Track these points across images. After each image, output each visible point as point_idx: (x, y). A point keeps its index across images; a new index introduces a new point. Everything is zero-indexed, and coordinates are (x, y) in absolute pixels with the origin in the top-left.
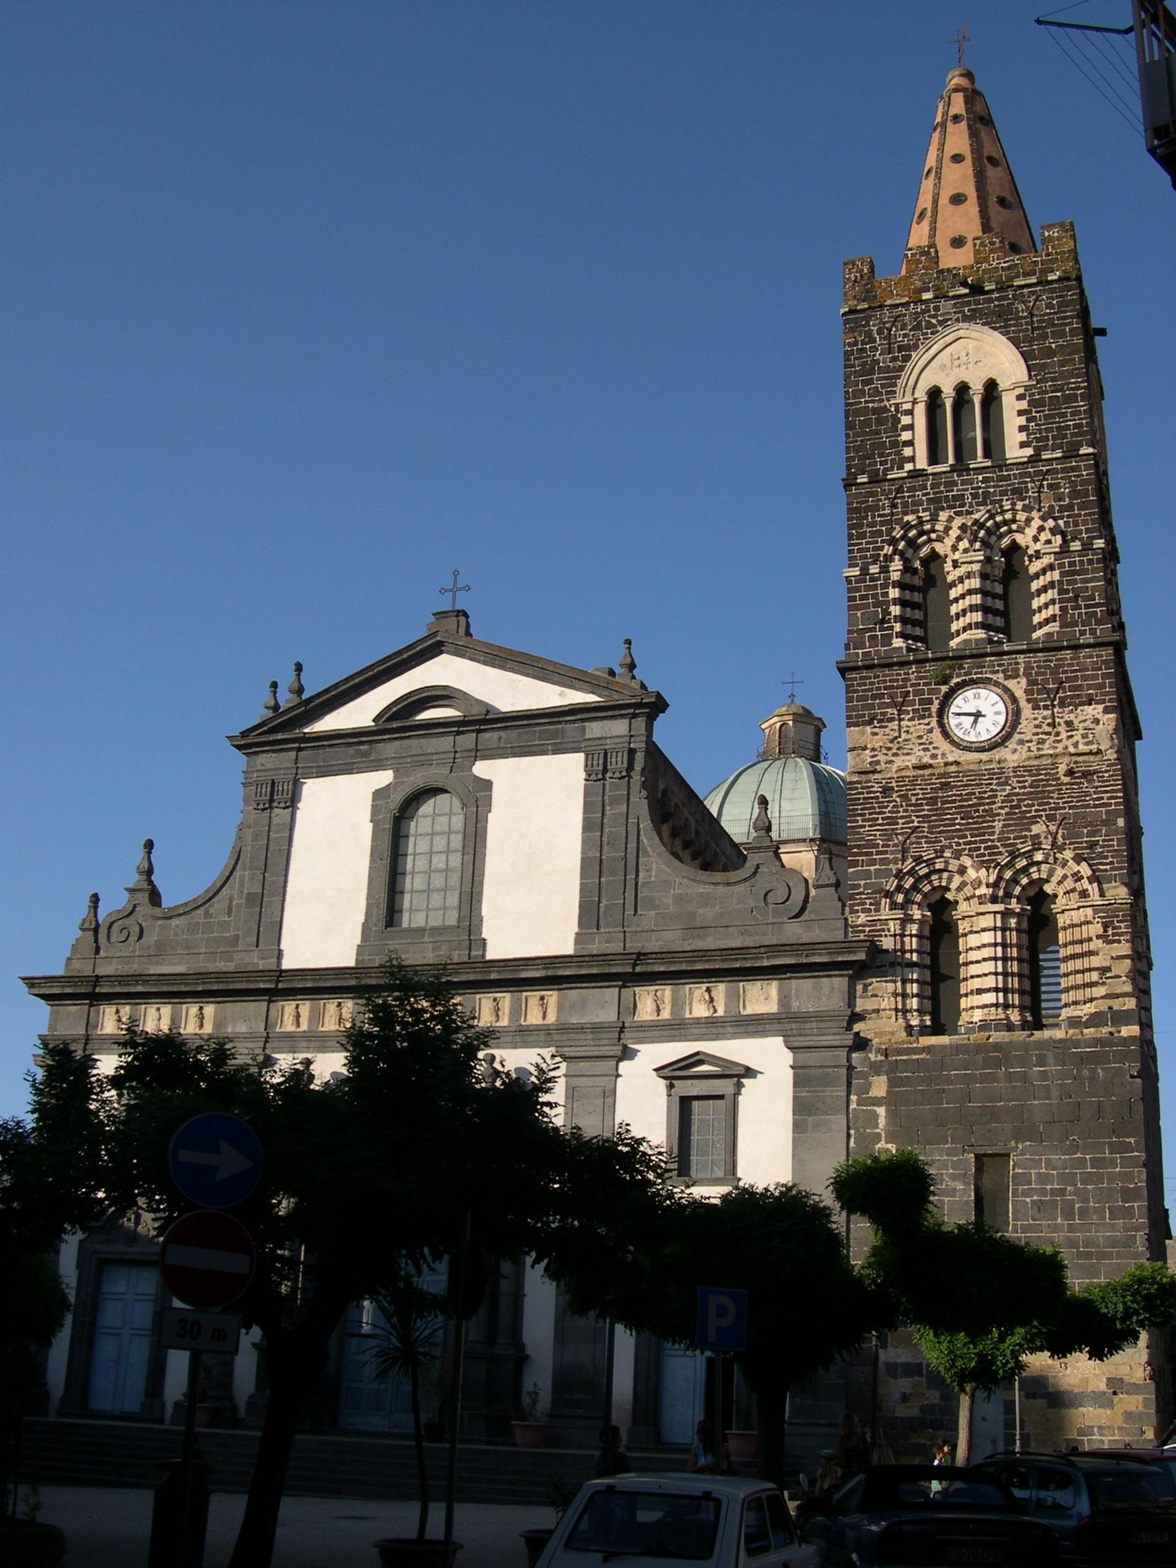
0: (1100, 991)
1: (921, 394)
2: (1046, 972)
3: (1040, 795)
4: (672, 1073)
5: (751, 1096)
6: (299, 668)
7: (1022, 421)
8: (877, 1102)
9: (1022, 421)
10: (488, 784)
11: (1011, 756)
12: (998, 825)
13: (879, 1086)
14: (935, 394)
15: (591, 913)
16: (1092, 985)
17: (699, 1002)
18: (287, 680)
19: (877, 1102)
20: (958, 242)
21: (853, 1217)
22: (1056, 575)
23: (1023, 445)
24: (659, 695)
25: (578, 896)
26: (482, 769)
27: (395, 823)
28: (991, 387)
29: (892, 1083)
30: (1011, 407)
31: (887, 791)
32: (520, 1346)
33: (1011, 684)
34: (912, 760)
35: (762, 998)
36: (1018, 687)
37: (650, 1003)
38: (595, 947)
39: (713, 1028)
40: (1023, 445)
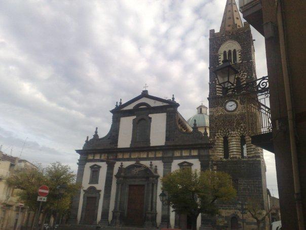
0: (253, 152)
1: (222, 52)
2: (231, 148)
3: (242, 119)
4: (180, 165)
5: (101, 169)
6: (121, 100)
7: (240, 56)
8: (215, 170)
9: (240, 56)
10: (150, 118)
11: (237, 112)
12: (235, 124)
13: (215, 168)
14: (225, 52)
15: (167, 139)
16: (252, 151)
17: (185, 153)
18: (119, 101)
19: (215, 170)
20: (229, 26)
21: (74, 181)
22: (245, 82)
23: (240, 60)
24: (119, 112)
25: (131, 136)
26: (150, 116)
27: (135, 123)
28: (235, 51)
29: (217, 167)
30: (238, 54)
31: (216, 119)
32: (156, 211)
33: (237, 101)
34: (220, 114)
35: (195, 153)
36: (238, 101)
37: (177, 154)
38: (169, 144)
39: (187, 157)
40: (240, 60)
